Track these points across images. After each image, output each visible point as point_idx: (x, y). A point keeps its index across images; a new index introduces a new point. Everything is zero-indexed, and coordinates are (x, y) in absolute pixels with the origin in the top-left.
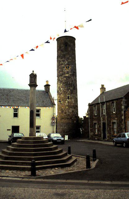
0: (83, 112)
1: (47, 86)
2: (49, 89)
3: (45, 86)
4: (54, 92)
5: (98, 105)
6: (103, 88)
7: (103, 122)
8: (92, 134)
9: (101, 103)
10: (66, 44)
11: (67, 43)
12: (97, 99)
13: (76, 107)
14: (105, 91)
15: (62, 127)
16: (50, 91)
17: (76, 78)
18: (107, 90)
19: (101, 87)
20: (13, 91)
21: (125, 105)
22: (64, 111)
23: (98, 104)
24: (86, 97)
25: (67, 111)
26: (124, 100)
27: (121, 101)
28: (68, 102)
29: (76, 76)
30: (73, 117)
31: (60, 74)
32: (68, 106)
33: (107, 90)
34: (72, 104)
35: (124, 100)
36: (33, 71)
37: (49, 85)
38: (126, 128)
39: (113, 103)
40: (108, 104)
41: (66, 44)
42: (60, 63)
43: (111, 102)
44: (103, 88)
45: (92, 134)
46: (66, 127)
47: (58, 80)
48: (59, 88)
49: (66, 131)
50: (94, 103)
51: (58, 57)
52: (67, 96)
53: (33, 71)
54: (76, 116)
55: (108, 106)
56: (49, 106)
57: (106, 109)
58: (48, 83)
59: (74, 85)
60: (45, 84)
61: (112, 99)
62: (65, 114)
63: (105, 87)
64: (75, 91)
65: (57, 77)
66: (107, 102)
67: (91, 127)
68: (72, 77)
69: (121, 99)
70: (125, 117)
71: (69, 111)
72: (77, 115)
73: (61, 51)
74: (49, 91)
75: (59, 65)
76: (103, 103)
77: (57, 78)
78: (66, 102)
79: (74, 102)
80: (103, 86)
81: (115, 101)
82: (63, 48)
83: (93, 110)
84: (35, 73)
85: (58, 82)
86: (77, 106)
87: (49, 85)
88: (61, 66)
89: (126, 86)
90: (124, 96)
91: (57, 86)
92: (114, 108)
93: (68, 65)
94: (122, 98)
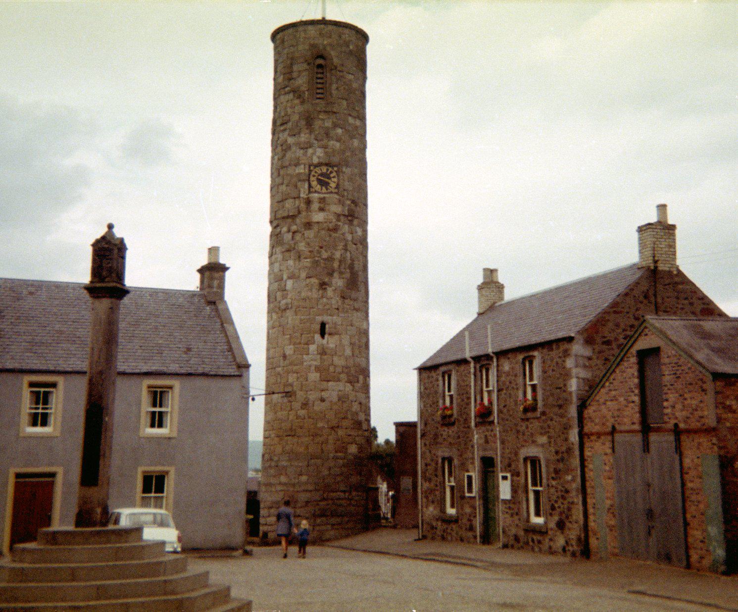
0: (393, 402)
1: (213, 271)
2: (221, 286)
3: (201, 271)
4: (248, 304)
5: (462, 368)
6: (490, 283)
7: (482, 454)
8: (431, 511)
9: (477, 359)
10: (320, 61)
11: (321, 57)
12: (458, 339)
13: (360, 376)
14: (502, 299)
15: (283, 479)
16: (226, 298)
17: (365, 232)
18: (509, 295)
19: (480, 280)
20: (31, 293)
21: (583, 374)
22: (300, 395)
23: (463, 362)
24: (409, 329)
25: (313, 396)
26: (578, 348)
27: (566, 353)
28: (323, 352)
29: (364, 223)
30: (345, 423)
31: (286, 219)
32: (317, 369)
33: (509, 295)
34: (339, 361)
35: (578, 348)
36: (110, 227)
37: (223, 269)
38: (589, 490)
39: (531, 360)
40: (506, 366)
41: (320, 61)
42: (289, 155)
43: (520, 357)
44: (490, 283)
45: (431, 511)
46: (304, 478)
47: (276, 238)
48: (276, 280)
49: (303, 497)
50: (442, 360)
51: (279, 124)
52: (319, 319)
53: (110, 227)
54: (359, 423)
55: (508, 374)
56: (268, 385)
57: (499, 391)
58: (217, 256)
59: (351, 267)
60: (204, 261)
61: (525, 342)
62: (302, 413)
63: (501, 278)
64: (354, 295)
65: (271, 222)
66: (502, 354)
67: (430, 480)
68: (346, 228)
69: (566, 346)
70: (581, 435)
71: (325, 394)
72: (362, 417)
73: (291, 96)
74: (221, 295)
75: (283, 167)
76: (482, 361)
77: (268, 229)
78: (313, 348)
79: (348, 352)
80: (490, 274)
81: (536, 353)
82: (302, 81)
83: (436, 392)
84: (118, 233)
85: (272, 247)
86: (365, 372)
87: (223, 269)
88: (290, 171)
89: (168, 294)
90: (578, 329)
91: (267, 268)
92: (534, 387)
93: (326, 165)
94: (570, 339)
